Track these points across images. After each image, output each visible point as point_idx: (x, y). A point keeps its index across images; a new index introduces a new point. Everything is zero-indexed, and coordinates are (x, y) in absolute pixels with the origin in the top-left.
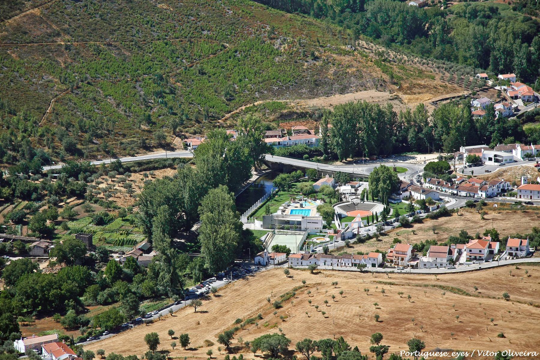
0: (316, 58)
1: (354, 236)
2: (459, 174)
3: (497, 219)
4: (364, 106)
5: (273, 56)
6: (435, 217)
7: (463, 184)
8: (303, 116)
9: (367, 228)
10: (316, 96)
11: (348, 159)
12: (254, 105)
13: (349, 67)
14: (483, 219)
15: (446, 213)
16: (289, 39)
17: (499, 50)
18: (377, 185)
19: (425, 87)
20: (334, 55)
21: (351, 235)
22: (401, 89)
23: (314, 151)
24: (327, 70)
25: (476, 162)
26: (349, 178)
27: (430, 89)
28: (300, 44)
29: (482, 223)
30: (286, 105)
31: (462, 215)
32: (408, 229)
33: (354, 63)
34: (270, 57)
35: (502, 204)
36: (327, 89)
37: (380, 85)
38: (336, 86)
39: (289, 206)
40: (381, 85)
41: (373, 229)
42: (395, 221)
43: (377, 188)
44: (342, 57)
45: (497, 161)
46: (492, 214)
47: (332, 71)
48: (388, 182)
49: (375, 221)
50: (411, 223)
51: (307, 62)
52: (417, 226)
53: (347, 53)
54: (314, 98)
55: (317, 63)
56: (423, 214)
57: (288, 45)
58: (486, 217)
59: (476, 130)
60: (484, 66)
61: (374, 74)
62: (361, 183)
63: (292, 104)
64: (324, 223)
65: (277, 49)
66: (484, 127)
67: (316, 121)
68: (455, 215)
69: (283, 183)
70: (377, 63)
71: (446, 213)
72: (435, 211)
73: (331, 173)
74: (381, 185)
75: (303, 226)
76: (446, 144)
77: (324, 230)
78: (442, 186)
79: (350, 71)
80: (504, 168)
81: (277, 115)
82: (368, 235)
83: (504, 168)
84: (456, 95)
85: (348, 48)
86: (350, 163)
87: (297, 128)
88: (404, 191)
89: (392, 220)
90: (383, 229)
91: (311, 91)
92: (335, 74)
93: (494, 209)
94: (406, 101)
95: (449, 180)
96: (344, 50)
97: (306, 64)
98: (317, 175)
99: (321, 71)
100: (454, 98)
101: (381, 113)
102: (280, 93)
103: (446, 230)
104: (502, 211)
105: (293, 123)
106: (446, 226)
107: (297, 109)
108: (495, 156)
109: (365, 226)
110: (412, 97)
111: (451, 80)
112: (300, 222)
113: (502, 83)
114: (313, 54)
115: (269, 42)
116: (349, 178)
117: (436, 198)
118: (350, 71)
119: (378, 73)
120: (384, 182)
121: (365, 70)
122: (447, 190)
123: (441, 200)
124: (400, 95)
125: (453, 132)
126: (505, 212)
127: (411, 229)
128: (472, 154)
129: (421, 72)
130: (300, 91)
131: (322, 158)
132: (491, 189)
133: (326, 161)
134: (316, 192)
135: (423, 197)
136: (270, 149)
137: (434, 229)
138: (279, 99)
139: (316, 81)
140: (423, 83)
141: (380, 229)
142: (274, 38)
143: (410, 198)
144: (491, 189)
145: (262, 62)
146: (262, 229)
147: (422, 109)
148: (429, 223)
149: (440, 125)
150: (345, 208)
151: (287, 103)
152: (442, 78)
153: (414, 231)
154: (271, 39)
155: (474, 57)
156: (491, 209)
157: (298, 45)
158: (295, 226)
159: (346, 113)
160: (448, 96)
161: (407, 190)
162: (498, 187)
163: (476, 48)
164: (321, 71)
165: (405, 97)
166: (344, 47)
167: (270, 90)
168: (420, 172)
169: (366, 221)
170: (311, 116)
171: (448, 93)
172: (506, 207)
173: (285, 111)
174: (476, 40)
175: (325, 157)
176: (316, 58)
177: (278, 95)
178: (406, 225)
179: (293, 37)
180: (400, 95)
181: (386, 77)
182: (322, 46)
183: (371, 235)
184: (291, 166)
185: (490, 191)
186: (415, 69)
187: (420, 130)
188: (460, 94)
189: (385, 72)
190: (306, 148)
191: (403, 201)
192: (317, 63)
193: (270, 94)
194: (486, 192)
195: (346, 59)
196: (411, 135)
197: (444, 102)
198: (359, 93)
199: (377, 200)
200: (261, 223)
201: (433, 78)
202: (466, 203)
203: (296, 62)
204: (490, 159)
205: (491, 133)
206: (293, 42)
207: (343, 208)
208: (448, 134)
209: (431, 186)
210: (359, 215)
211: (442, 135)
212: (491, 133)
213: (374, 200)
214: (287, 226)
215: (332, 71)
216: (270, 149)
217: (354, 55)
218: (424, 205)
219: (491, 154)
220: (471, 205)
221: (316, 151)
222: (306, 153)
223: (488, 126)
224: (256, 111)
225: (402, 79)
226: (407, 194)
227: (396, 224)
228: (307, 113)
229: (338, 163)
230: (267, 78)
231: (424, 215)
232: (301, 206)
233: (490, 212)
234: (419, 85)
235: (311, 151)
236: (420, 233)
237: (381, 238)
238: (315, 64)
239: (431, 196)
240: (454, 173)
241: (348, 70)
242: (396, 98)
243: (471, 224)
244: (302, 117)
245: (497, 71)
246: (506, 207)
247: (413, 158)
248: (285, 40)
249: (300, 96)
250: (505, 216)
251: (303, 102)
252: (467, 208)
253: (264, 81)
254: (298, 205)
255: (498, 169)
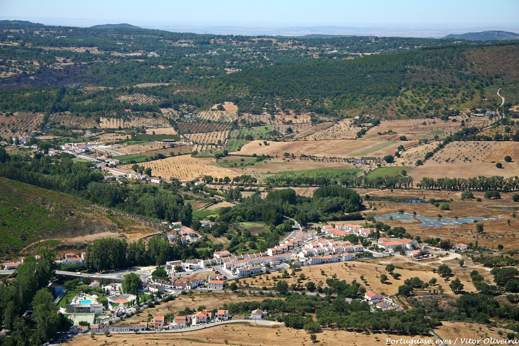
0: (72, 215)
1: (123, 314)
2: (173, 277)
3: (200, 301)
4: (112, 240)
5: (46, 214)
6: (166, 301)
7: (176, 282)
8: (70, 247)
9: (129, 309)
10: (76, 236)
11: (103, 271)
12: (40, 242)
13: (93, 219)
14: (193, 300)
15: (172, 298)
16: (54, 204)
17: (170, 209)
18: (130, 284)
19: (137, 229)
20: (82, 213)
21: (121, 314)
22: (124, 231)
23: (81, 267)
24: (80, 221)
25: (179, 269)
26: (109, 282)
27: (140, 230)
28: (61, 207)
29: (193, 303)
30: (59, 242)
31: (180, 299)
32: (153, 308)
33: (95, 217)
34: (45, 215)
35: (201, 292)
36: (82, 232)
37: (112, 229)
38: (87, 230)
39: (77, 299)
40: (113, 229)
41: (133, 310)
42: (144, 304)
43: (130, 286)
44: (87, 214)
45: (191, 269)
46: (197, 298)
47: (83, 221)
48: (136, 282)
49: (133, 305)
50: (154, 305)
51: (67, 217)
52: (157, 306)
53: (90, 212)
54: (75, 237)
55: (74, 218)
56: (158, 300)
57: (54, 208)
58: (194, 299)
59: (173, 252)
60: (162, 218)
61: (107, 223)
62: (116, 284)
63: (63, 241)
64: (104, 307)
65: (48, 210)
66: (177, 250)
67: (79, 250)
68: (177, 299)
69: (70, 286)
70: (107, 216)
71: (172, 298)
72: (166, 297)
73: (97, 279)
74: (132, 284)
75: (91, 310)
76: (157, 260)
77: (105, 312)
78: (165, 283)
79: (93, 221)
80: (196, 272)
81: (55, 247)
82: (132, 313)
83: (196, 272)
84: (155, 233)
85: (89, 208)
86: (104, 273)
87: (69, 254)
88: (145, 287)
89: (143, 303)
90: (140, 309)
91: (73, 233)
92: (85, 223)
93: (198, 295)
94: (129, 237)
95: (168, 280)
96: (88, 210)
97: (67, 218)
98: (88, 281)
99: (76, 221)
100: (154, 235)
101: (121, 244)
102: (54, 234)
103: (174, 308)
104: (202, 296)
105: (65, 252)
106: (174, 305)
107: (67, 243)
108: (190, 266)
109: (128, 308)
110: (132, 235)
111: (150, 225)
112: (89, 307)
113: (176, 227)
114: (70, 213)
115: (42, 206)
116: (109, 282)
117: (164, 290)
118: (93, 221)
119: (109, 222)
120: (134, 282)
121: (102, 220)
122: (168, 286)
123: (166, 291)
124: (125, 234)
125: (161, 253)
126: (204, 296)
127: (154, 308)
128: (178, 265)
129: (133, 221)
130: (66, 233)
131: (87, 271)
132: (193, 284)
133: (89, 272)
134: (91, 290)
135: (157, 290)
136: (58, 267)
137: (169, 307)
138: (54, 238)
139: (75, 227)
140: (136, 227)
141: (138, 309)
142: (45, 204)
143: (148, 291)
144: (193, 284)
145: (40, 217)
146: (66, 313)
147: (140, 241)
148: (164, 305)
149: (153, 250)
150: (113, 298)
151: (60, 241)
152: (145, 225)
153: (157, 310)
154: (43, 204)
155: (155, 213)
156: (196, 295)
157: (60, 208)
158: (86, 310)
159: (102, 244)
160: (151, 234)
161: (146, 287)
162: (197, 283)
163: (156, 208)
164: (76, 221)
165: (128, 235)
166: (87, 208)
167: (48, 233)
168: (150, 276)
169: (127, 305)
170: (75, 247)
171: (150, 232)
172: (203, 294)
173: (60, 245)
174: (156, 204)
175: (88, 271)
176: (72, 215)
177: (53, 236)
178: (151, 306)
179: (56, 203)
180: (125, 234)
181: (116, 225)
182: (74, 208)
183: (134, 313)
184: (70, 276)
185: (193, 286)
186: (129, 220)
187: (142, 253)
188: (157, 233)
189: (113, 221)
190: (77, 266)
191: (145, 293)
192: (74, 218)
193: (48, 235)
194: (191, 286)
195: (90, 215)
196: (137, 256)
197: (149, 238)
198: (101, 233)
199: (130, 293)
200: (65, 309)
201: (140, 225)
202: (181, 292)
203: (61, 217)
204: (187, 268)
205: (181, 254)
206: (57, 206)
207: (111, 298)
208: (158, 255)
209: (158, 284)
210: (121, 302)
211: (155, 256)
212: (181, 254)
213: (128, 293)
214: (80, 310)
215: (83, 221)
216: (58, 267)
217: (94, 213)
218: (159, 294)
219: (187, 265)
220: (184, 293)
221: (83, 267)
222: (77, 269)
223: (179, 250)
224: (41, 245)
225: (124, 225)
226: (146, 289)
227: (145, 306)
228: (73, 246)
229: (97, 273)
230: (45, 226)
231: (159, 300)
232: (85, 298)
233: (195, 297)
234: (134, 228)
235: (80, 267)
236: (160, 310)
237: (139, 314)
238: (72, 218)
239: (161, 290)
240: (169, 276)
241: (92, 221)
242: (123, 236)
243: (188, 304)
244: (70, 248)
245: (171, 222)
246: (203, 294)
247: (140, 269)
248: (52, 205)
249: (66, 236)
250: (204, 298)
251: (69, 240)
252: (182, 295)
253: (43, 228)
254: (83, 298)
255: (193, 273)
